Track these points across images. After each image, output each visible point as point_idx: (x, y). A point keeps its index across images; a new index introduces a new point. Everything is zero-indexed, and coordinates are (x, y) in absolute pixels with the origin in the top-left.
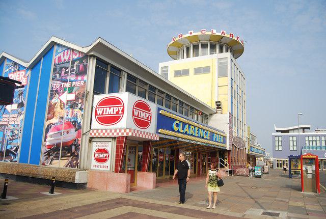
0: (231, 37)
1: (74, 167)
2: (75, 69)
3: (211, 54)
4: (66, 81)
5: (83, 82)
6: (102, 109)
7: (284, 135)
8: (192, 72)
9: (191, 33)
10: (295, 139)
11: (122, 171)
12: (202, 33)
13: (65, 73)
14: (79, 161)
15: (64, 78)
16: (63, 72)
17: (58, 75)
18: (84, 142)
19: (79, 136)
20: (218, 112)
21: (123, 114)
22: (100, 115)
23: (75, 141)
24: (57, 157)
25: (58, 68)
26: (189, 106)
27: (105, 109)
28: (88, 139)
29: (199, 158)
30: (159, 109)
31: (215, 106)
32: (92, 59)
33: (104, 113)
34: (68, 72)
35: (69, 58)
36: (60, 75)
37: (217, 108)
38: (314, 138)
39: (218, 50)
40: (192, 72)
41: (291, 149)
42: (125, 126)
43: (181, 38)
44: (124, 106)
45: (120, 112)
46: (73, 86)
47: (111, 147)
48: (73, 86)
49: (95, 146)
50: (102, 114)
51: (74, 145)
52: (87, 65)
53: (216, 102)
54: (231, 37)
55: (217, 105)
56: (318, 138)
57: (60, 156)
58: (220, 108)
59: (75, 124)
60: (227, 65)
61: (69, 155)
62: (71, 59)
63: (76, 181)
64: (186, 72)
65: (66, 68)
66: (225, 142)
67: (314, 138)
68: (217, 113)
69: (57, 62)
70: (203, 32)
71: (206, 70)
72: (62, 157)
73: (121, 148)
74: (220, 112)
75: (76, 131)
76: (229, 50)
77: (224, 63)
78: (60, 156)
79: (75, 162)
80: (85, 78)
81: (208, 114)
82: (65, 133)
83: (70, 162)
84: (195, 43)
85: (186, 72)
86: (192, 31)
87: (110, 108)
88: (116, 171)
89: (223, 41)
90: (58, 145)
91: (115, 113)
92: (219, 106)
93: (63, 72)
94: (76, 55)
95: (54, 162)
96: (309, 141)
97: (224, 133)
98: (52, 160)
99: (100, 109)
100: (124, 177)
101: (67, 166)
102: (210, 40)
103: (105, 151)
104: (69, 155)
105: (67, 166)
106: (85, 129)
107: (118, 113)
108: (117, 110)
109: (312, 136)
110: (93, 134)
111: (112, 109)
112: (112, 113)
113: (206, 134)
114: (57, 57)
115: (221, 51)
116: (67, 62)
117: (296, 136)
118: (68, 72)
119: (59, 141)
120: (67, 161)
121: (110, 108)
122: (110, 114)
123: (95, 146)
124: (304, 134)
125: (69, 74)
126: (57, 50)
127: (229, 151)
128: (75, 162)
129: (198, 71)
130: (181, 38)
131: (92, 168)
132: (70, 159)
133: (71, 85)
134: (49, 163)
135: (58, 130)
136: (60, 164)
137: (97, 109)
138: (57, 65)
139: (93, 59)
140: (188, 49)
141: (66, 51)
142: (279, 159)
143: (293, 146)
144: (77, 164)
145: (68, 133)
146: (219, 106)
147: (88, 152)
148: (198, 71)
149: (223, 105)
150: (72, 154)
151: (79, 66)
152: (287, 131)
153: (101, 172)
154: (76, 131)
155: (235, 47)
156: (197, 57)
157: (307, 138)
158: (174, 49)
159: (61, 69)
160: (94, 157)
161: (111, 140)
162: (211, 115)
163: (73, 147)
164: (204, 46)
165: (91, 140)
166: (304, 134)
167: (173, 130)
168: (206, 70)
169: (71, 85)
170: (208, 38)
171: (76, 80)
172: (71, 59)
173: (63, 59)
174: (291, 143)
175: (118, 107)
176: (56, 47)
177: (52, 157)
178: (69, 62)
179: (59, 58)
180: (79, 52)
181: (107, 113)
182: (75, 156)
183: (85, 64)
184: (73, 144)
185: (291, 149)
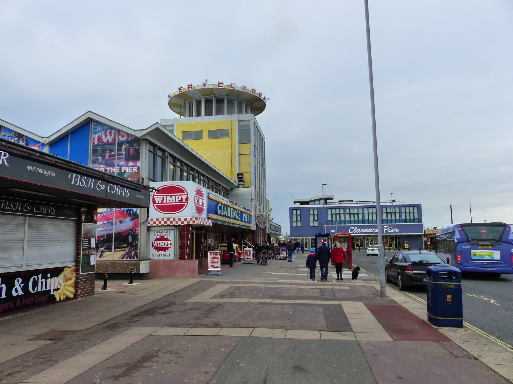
1: (133, 257)
2: (124, 152)
3: (216, 115)
4: (113, 166)
5: (136, 168)
6: (162, 197)
8: (205, 135)
10: (316, 212)
11: (191, 257)
12: (219, 86)
13: (110, 156)
14: (138, 251)
15: (109, 162)
16: (107, 155)
17: (100, 158)
18: (142, 231)
19: (136, 225)
20: (240, 186)
21: (187, 203)
22: (159, 203)
23: (132, 230)
24: (109, 249)
25: (99, 149)
26: (214, 181)
27: (165, 197)
28: (146, 228)
30: (209, 194)
31: (234, 180)
33: (165, 201)
34: (114, 155)
35: (114, 139)
36: (103, 157)
37: (239, 181)
38: (338, 211)
39: (236, 110)
40: (205, 135)
41: (312, 225)
42: (188, 215)
43: (190, 89)
44: (187, 195)
45: (184, 201)
46: (123, 171)
47: (172, 235)
48: (123, 171)
49: (153, 236)
50: (162, 202)
51: (131, 235)
52: (139, 149)
53: (238, 174)
54: (253, 94)
55: (239, 178)
56: (342, 211)
57: (113, 248)
59: (130, 213)
60: (249, 130)
61: (125, 245)
62: (117, 140)
63: (141, 272)
64: (197, 135)
65: (111, 151)
66: (250, 222)
67: (338, 211)
68: (238, 187)
69: (96, 142)
70: (221, 85)
71: (223, 134)
72: (115, 248)
75: (131, 220)
76: (249, 110)
77: (245, 126)
78: (113, 248)
79: (133, 252)
80: (139, 164)
81: (229, 189)
82: (118, 223)
83: (127, 253)
85: (197, 135)
87: (171, 196)
88: (183, 258)
90: (109, 236)
91: (177, 201)
92: (241, 177)
93: (107, 155)
94: (123, 136)
95: (104, 254)
96: (332, 214)
97: (249, 210)
98: (102, 252)
99: (159, 197)
101: (123, 258)
102: (227, 95)
103: (166, 240)
104: (125, 245)
105: (123, 258)
106: (142, 218)
107: (181, 201)
108: (180, 199)
109: (336, 208)
110: (152, 223)
111: (173, 197)
112: (174, 201)
113: (238, 214)
114: (96, 136)
116: (111, 144)
117: (317, 208)
118: (114, 155)
119: (110, 232)
120: (123, 252)
121: (171, 196)
122: (172, 203)
123: (153, 236)
124: (325, 206)
125: (116, 157)
126: (95, 129)
128: (133, 252)
129: (213, 134)
130: (190, 89)
131: (151, 257)
132: (127, 250)
133: (121, 170)
134: (99, 256)
135: (107, 219)
136: (115, 256)
137: (155, 197)
138: (97, 145)
139: (146, 145)
140: (199, 103)
141: (108, 131)
142: (297, 238)
143: (314, 221)
144: (136, 255)
145: (121, 222)
146: (241, 177)
147: (146, 242)
148: (213, 134)
149: (246, 178)
150: (129, 244)
151: (129, 149)
152: (307, 203)
153: (165, 261)
154: (131, 220)
155: (256, 105)
156: (230, 116)
157: (329, 212)
158: (180, 101)
159: (104, 151)
160: (153, 245)
161: (173, 228)
162: (232, 189)
163: (130, 238)
165: (149, 229)
166: (325, 206)
167: (216, 213)
168: (223, 134)
169: (121, 170)
171: (127, 166)
172: (117, 140)
173: (105, 140)
174: (312, 218)
175: (181, 195)
176: (92, 127)
177: (101, 249)
178: (114, 144)
179: (100, 138)
180: (128, 134)
181: (168, 201)
182: (133, 246)
183: (137, 148)
184: (129, 234)
185: (312, 225)
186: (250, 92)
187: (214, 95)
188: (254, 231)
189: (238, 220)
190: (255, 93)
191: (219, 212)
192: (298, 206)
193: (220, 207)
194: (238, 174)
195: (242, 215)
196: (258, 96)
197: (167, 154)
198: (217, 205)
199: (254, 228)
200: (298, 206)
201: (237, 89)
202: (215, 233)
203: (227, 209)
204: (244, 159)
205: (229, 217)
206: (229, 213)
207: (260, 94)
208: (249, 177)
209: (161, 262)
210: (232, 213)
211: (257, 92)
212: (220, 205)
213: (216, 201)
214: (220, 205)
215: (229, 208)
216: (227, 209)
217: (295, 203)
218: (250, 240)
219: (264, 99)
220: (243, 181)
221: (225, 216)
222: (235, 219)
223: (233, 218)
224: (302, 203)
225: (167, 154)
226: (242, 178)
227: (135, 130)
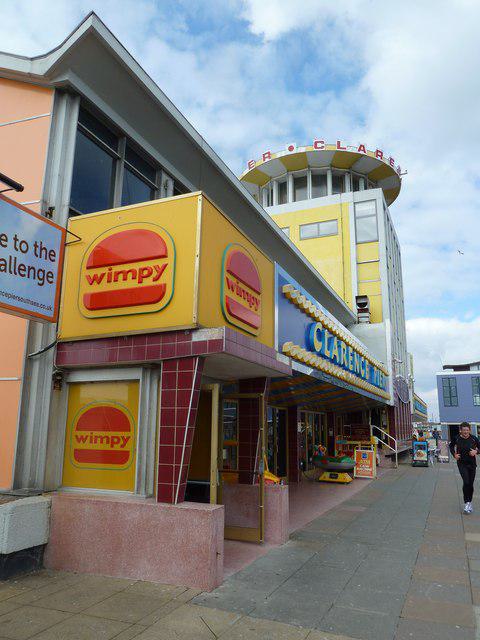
0: (379, 158)
3: (314, 197)
7: (195, 245)
9: (291, 148)
11: (197, 493)
12: (316, 147)
29: (330, 426)
32: (40, 477)
37: (359, 311)
39: (348, 185)
43: (267, 160)
53: (357, 298)
54: (379, 158)
55: (359, 305)
58: (366, 311)
70: (319, 145)
73: (184, 401)
74: (367, 320)
84: (299, 173)
86: (294, 145)
89: (360, 167)
100: (203, 521)
102: (332, 166)
115: (356, 188)
127: (391, 409)
130: (267, 160)
140: (282, 187)
146: (362, 304)
149: (372, 304)
152: (466, 367)
156: (337, 196)
164: (319, 180)
167: (310, 348)
170: (328, 160)
186: (374, 156)
187: (309, 166)
188: (393, 407)
189: (364, 379)
190: (381, 156)
191: (318, 346)
192: (451, 372)
193: (320, 335)
194: (357, 298)
195: (371, 370)
196: (387, 163)
197: (164, 177)
198: (309, 328)
199: (391, 402)
200: (451, 372)
201: (349, 150)
202: (315, 408)
203: (339, 346)
204: (366, 270)
205: (343, 367)
206: (344, 356)
207: (392, 160)
208: (378, 302)
209: (87, 508)
210: (351, 358)
211: (386, 156)
212: (319, 326)
213: (309, 315)
214: (319, 326)
215: (343, 345)
216: (339, 346)
217: (445, 367)
218: (385, 427)
219: (399, 170)
220: (366, 311)
221: (333, 361)
222: (359, 375)
223: (353, 372)
224: (457, 368)
225: (164, 177)
226: (365, 304)
227: (32, 59)
